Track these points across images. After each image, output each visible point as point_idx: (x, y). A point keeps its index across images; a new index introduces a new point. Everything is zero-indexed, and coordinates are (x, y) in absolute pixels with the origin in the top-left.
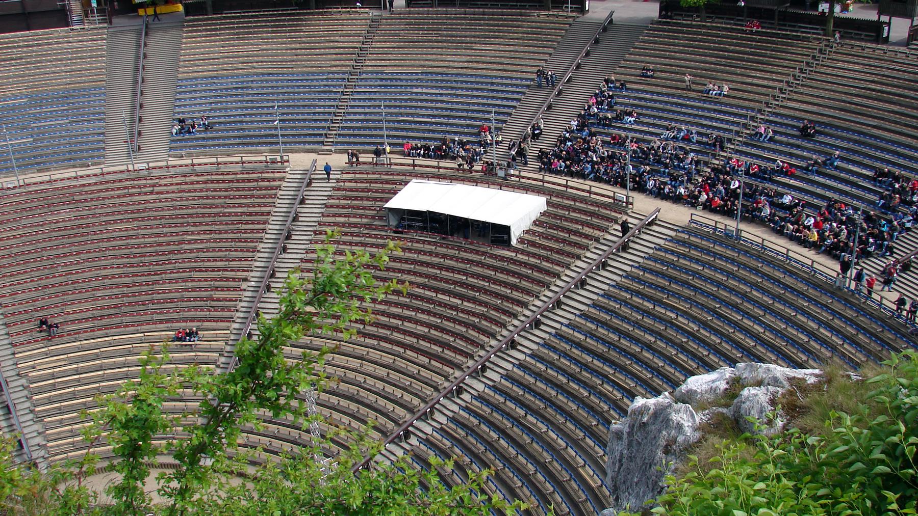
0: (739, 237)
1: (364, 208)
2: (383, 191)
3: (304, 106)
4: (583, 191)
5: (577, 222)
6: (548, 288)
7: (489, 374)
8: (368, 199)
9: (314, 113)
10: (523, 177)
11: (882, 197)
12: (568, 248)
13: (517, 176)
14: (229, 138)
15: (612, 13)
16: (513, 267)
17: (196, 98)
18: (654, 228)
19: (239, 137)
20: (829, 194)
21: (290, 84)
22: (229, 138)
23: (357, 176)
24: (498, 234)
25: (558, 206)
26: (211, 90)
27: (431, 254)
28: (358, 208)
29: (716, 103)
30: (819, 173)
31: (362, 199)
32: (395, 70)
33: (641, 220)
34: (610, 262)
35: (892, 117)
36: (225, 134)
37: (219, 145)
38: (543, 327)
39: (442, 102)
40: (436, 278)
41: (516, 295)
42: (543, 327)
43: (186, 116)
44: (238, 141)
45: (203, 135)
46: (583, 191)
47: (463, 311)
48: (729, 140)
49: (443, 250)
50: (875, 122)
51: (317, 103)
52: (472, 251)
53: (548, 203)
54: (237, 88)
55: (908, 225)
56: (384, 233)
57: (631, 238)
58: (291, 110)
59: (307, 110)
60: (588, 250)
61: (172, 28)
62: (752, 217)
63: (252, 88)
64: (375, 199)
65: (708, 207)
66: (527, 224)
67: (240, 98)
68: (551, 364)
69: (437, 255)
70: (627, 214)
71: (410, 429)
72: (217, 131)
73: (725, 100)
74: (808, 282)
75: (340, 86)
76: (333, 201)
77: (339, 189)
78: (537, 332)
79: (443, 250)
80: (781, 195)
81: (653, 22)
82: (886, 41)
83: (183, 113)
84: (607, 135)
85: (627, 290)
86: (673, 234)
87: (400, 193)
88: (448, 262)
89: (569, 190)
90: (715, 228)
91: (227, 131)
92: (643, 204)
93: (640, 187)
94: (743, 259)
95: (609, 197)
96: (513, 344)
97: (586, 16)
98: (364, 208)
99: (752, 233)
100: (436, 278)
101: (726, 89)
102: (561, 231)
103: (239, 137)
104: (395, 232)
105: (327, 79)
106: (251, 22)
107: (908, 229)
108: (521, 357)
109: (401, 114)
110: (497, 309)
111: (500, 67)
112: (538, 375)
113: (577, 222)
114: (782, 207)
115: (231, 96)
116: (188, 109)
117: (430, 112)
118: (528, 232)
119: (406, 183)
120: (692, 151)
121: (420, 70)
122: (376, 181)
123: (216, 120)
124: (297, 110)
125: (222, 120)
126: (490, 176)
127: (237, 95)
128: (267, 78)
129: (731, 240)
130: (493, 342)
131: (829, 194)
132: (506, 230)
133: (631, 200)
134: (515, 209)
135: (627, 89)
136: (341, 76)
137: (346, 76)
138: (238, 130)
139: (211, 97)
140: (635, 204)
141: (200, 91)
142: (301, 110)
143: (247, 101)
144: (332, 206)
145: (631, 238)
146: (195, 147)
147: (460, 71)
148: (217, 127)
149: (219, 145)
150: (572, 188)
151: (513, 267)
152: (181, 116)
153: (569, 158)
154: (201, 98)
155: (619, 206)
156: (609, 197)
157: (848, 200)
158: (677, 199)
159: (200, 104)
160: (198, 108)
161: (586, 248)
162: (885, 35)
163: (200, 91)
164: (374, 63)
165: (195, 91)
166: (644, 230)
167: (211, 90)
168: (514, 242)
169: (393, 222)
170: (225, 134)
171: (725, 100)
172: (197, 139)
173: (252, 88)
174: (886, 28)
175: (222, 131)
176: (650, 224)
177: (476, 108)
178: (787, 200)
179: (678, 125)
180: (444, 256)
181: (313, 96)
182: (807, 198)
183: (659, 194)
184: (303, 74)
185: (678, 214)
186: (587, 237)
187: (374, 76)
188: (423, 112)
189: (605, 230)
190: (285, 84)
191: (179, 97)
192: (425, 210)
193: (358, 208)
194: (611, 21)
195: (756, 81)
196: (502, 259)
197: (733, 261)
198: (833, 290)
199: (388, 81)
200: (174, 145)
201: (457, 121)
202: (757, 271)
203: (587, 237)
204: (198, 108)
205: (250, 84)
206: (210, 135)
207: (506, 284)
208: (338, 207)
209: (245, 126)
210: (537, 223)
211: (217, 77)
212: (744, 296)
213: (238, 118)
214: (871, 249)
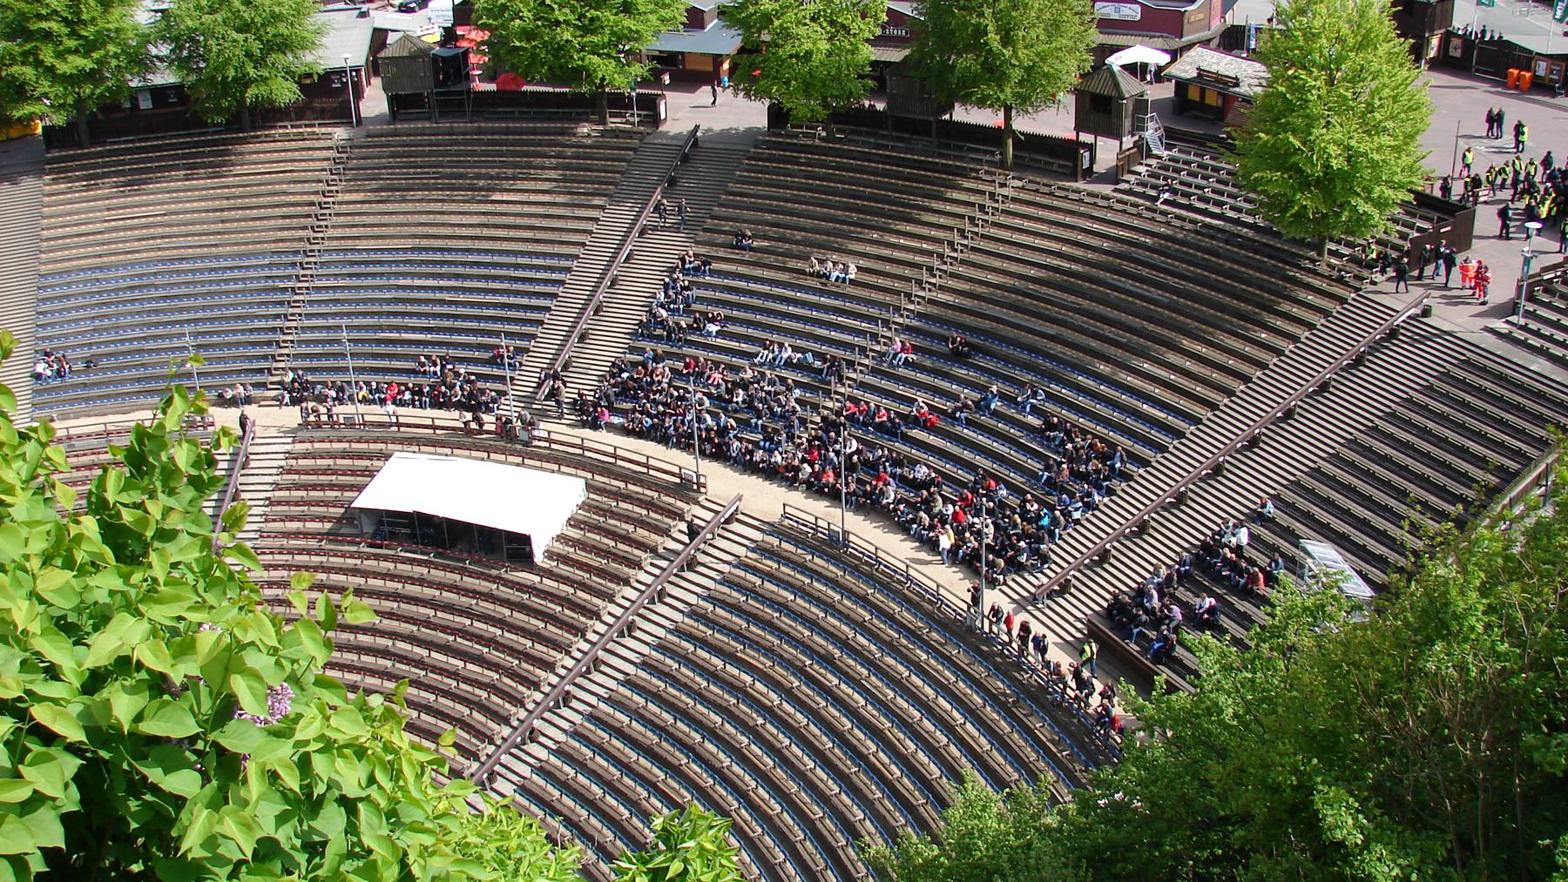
0: (846, 543)
1: (326, 504)
2: (354, 473)
3: (237, 318)
4: (638, 463)
5: (627, 519)
6: (583, 636)
7: (500, 785)
8: (332, 487)
9: (252, 331)
10: (555, 442)
11: (1048, 468)
12: (614, 566)
13: (546, 440)
14: (122, 382)
15: (697, 127)
16: (536, 602)
17: (68, 310)
18: (735, 526)
19: (139, 380)
20: (979, 460)
21: (214, 276)
22: (122, 382)
23: (317, 445)
24: (515, 547)
25: (601, 491)
26: (92, 294)
27: (421, 581)
28: (318, 503)
29: (837, 296)
30: (970, 423)
31: (323, 487)
32: (372, 244)
33: (717, 513)
34: (640, 622)
35: (1079, 320)
36: (118, 375)
37: (108, 397)
38: (638, 634)
39: (442, 302)
40: (428, 624)
41: (540, 649)
42: (638, 634)
43: (56, 343)
44: (137, 387)
45: (83, 379)
46: (638, 463)
47: (467, 680)
48: (851, 364)
49: (438, 575)
50: (1052, 329)
51: (256, 311)
52: (480, 576)
53: (590, 487)
54: (132, 288)
55: (1077, 515)
56: (354, 549)
57: (702, 546)
58: (216, 327)
59: (240, 325)
60: (641, 568)
61: (27, 173)
62: (869, 504)
63: (156, 287)
64: (342, 487)
65: (815, 488)
66: (558, 526)
67: (138, 307)
68: (581, 766)
69: (431, 584)
70: (698, 503)
71: (497, 768)
72: (105, 370)
73: (851, 290)
74: (929, 617)
75: (289, 277)
76: (282, 493)
77: (289, 472)
78: (628, 642)
79: (438, 575)
80: (914, 463)
81: (764, 134)
82: (1088, 173)
83: (50, 338)
84: (681, 357)
85: (689, 637)
86: (757, 535)
87: (379, 476)
88: (449, 596)
89: (620, 463)
90: (816, 528)
91: (121, 369)
92: (722, 482)
93: (720, 454)
94: (849, 580)
95: (673, 474)
96: (533, 735)
97: (662, 128)
98: (326, 504)
99: (866, 533)
100: (428, 624)
101: (852, 269)
102: (623, 519)
103: (139, 380)
104: (371, 546)
105: (270, 266)
106: (151, 160)
107: (1077, 522)
108: (543, 754)
109: (381, 328)
110: (513, 675)
111: (529, 234)
112: (565, 786)
113: (627, 519)
114: (916, 485)
115: (124, 303)
116: (57, 331)
117: (423, 323)
118: (562, 538)
119: (387, 457)
120: (798, 384)
121: (409, 243)
122: (344, 455)
123: (103, 350)
124: (226, 327)
125: (112, 348)
126: (510, 442)
127: (133, 301)
128: (178, 266)
129: (834, 545)
130: (506, 731)
131: (979, 460)
132: (525, 540)
133: (702, 480)
134: (533, 502)
135: (713, 273)
136: (291, 259)
137: (299, 259)
138: (137, 367)
139: (93, 306)
140: (709, 485)
141: (76, 296)
142: (232, 326)
143: (149, 312)
144: (279, 503)
145: (702, 546)
146: (71, 401)
147: (469, 244)
148: (104, 362)
149: (108, 397)
150: (623, 459)
151: (536, 602)
152: (47, 346)
153: (628, 397)
154: (77, 309)
155: (687, 488)
156: (673, 474)
157: (1002, 471)
158: (771, 473)
159: (76, 321)
160: (73, 328)
161: (637, 565)
162: (1086, 165)
163: (76, 296)
164: (339, 232)
165: (68, 297)
166: (721, 532)
167: (92, 294)
168: (539, 558)
169: (368, 528)
170: (118, 375)
171: (851, 290)
172: (75, 386)
173: (156, 287)
174: (1087, 154)
175: (113, 370)
176: (727, 521)
177: (491, 312)
178: (922, 472)
179: (780, 339)
180: (441, 586)
181: (249, 299)
182: (949, 468)
183: (748, 466)
184: (233, 256)
185: (767, 500)
186: (641, 545)
187: (341, 257)
188: (414, 322)
189: (665, 532)
190: (207, 277)
191: (43, 308)
192: (409, 509)
193: (318, 503)
194: (696, 141)
195: (897, 254)
196: (521, 587)
197: (833, 583)
198: (962, 631)
199: (361, 267)
200: (39, 399)
201: (463, 339)
202: (864, 601)
203: (641, 545)
204: (73, 328)
205: (152, 280)
206: (94, 378)
207: (512, 651)
208: (288, 503)
209: (147, 359)
210: (574, 522)
211: (101, 268)
212: (844, 645)
213: (136, 345)
214: (1023, 559)
